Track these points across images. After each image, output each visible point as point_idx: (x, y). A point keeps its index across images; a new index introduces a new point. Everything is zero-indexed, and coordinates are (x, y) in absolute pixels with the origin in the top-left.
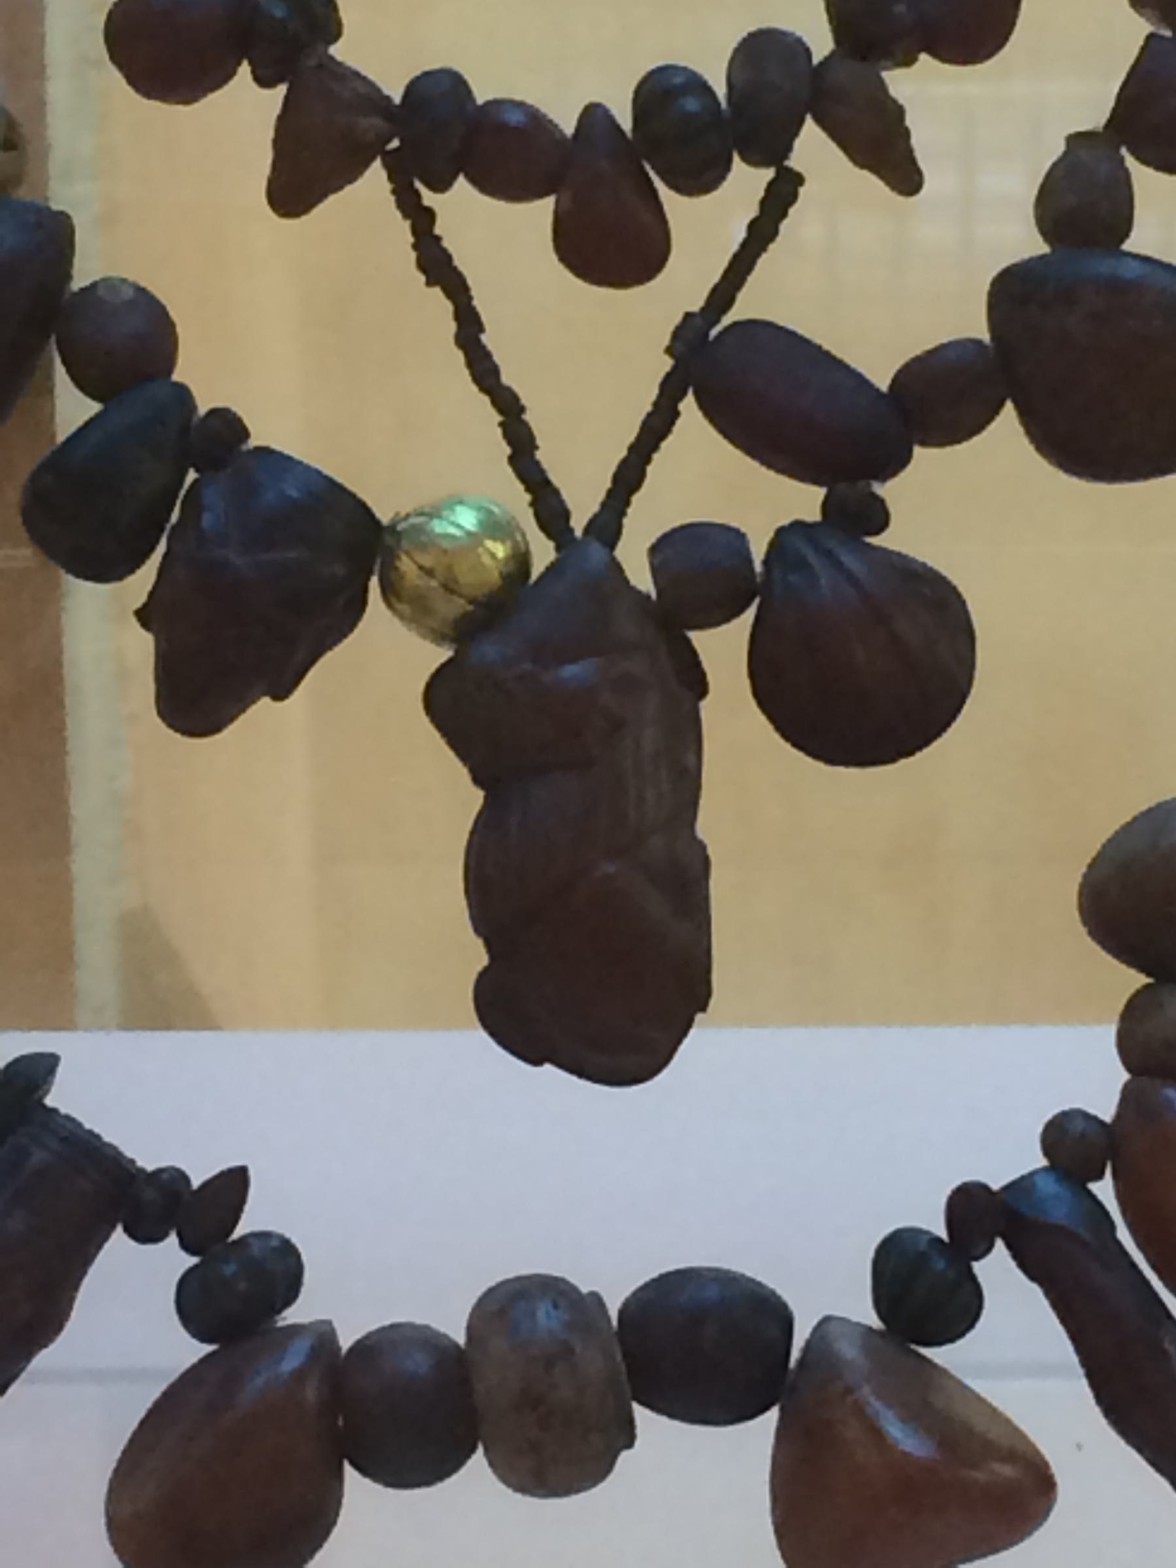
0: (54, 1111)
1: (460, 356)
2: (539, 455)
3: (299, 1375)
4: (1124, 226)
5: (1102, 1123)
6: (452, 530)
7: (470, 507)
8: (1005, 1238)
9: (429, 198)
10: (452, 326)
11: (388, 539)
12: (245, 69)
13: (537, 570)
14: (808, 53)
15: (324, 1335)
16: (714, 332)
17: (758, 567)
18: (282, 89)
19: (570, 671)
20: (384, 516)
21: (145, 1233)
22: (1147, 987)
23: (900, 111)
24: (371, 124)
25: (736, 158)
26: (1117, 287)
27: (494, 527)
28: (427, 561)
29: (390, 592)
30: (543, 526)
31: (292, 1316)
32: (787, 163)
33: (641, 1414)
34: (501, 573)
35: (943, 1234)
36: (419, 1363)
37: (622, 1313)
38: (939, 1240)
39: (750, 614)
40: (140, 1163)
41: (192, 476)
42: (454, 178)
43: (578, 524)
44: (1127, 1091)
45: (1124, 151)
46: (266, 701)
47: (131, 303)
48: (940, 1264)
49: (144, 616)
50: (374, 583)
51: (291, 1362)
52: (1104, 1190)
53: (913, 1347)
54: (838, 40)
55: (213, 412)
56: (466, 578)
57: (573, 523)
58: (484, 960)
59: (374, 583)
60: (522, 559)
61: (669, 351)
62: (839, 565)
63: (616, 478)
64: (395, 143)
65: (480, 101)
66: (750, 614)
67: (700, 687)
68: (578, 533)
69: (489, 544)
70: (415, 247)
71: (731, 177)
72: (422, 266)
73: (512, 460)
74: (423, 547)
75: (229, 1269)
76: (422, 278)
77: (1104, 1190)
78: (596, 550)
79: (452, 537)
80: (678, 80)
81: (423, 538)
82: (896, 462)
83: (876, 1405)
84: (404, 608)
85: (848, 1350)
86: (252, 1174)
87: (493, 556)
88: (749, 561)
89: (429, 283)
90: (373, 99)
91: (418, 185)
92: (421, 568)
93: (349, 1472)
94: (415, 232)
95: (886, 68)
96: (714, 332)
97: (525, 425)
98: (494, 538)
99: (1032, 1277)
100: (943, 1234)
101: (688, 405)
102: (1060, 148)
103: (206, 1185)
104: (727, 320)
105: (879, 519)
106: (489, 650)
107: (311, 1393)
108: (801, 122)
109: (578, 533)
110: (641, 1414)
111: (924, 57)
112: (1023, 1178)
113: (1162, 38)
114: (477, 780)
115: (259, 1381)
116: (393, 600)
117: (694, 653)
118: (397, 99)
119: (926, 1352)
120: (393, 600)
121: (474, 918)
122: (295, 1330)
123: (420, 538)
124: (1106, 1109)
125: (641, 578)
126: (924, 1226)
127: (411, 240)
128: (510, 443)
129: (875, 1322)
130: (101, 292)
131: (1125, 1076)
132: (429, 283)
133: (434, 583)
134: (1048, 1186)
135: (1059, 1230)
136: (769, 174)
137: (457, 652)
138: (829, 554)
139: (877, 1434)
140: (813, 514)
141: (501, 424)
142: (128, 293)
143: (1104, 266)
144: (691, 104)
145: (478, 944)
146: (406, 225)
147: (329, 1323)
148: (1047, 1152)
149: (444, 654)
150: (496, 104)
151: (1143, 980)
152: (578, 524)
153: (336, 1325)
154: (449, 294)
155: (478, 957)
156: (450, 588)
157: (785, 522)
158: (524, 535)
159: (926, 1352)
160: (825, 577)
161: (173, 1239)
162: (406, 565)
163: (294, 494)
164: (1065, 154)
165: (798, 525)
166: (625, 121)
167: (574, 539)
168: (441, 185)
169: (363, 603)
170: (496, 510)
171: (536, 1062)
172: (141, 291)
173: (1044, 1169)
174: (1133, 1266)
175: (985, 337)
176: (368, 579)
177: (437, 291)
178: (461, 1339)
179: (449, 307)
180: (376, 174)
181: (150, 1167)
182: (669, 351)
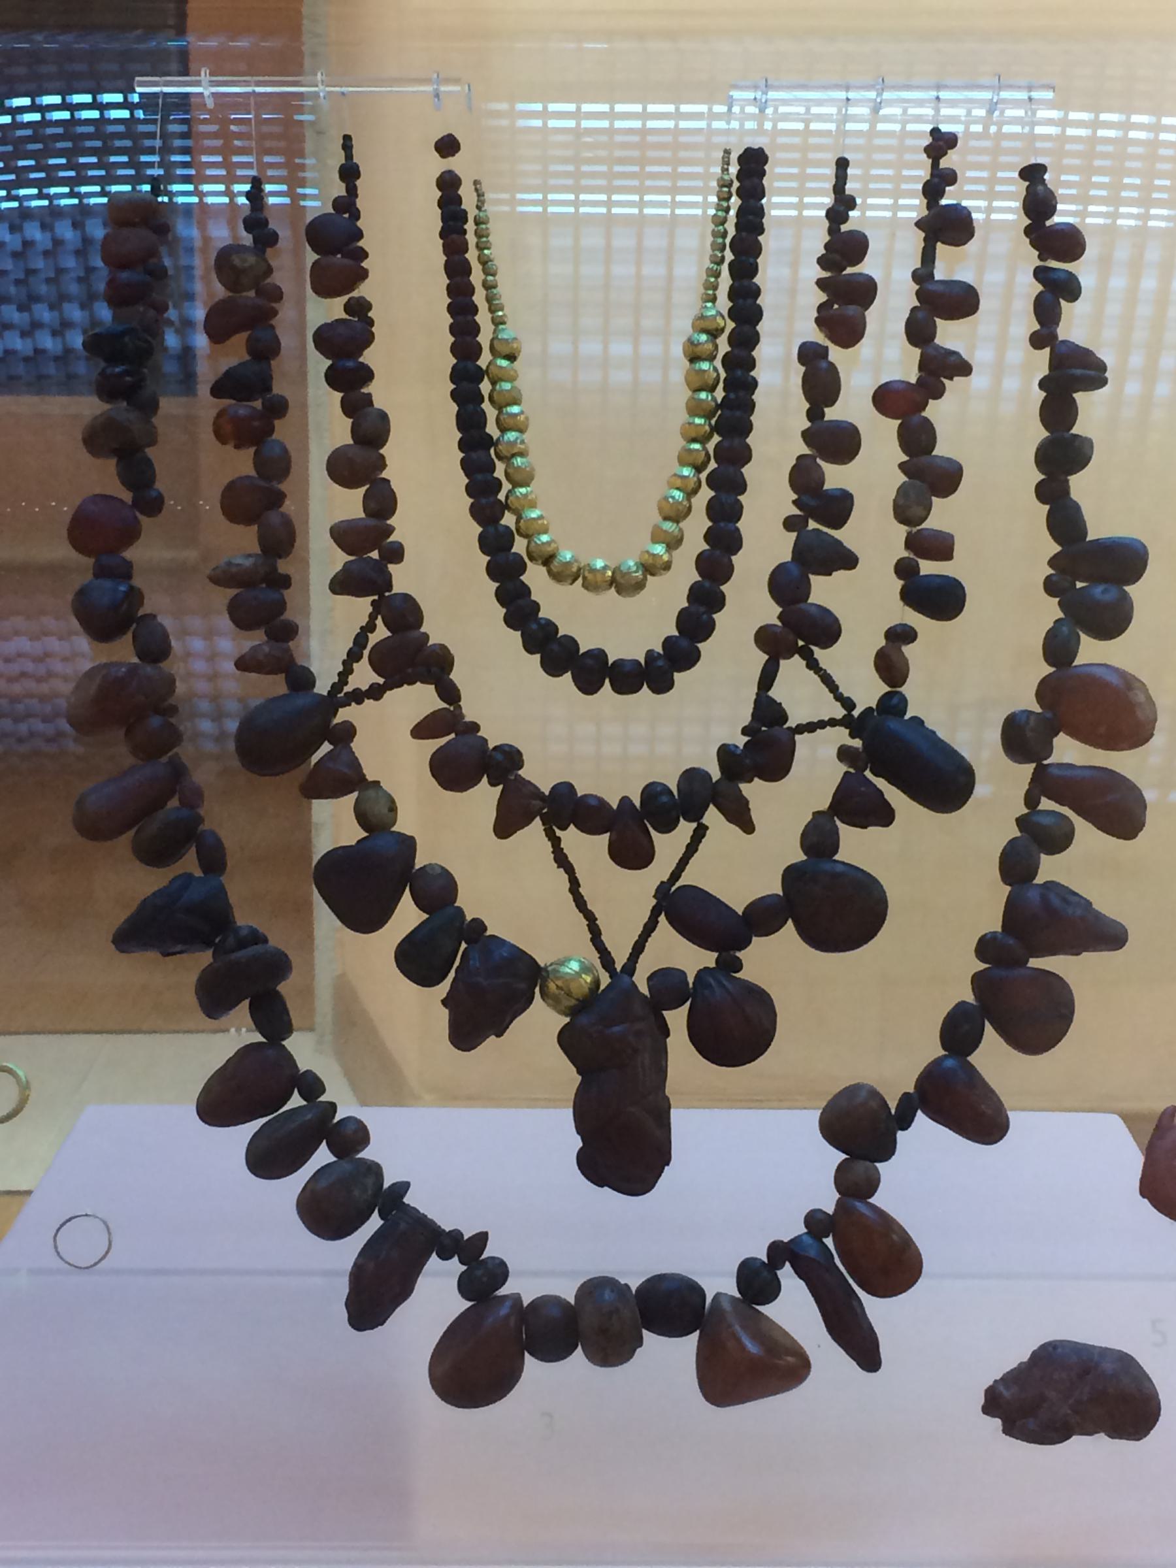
0: (408, 1205)
1: (571, 897)
2: (603, 938)
3: (507, 1317)
4: (835, 850)
5: (829, 1214)
6: (569, 971)
7: (575, 961)
8: (790, 1262)
9: (558, 833)
10: (568, 885)
11: (544, 974)
12: (485, 779)
13: (602, 987)
14: (711, 778)
15: (517, 1298)
16: (673, 889)
17: (691, 985)
18: (501, 787)
19: (616, 1029)
20: (542, 965)
21: (445, 1256)
22: (846, 1159)
23: (747, 802)
24: (537, 803)
25: (681, 819)
26: (835, 876)
27: (586, 969)
28: (560, 983)
29: (544, 995)
30: (604, 967)
31: (503, 1291)
32: (701, 821)
33: (645, 1332)
34: (589, 988)
35: (766, 1260)
36: (555, 1312)
37: (636, 1291)
38: (764, 1262)
39: (688, 1004)
40: (443, 1227)
41: (464, 946)
42: (569, 825)
43: (619, 967)
44: (839, 1202)
45: (836, 818)
46: (493, 1037)
47: (440, 875)
48: (765, 1274)
49: (445, 1002)
50: (537, 990)
51: (504, 1311)
52: (829, 1242)
53: (754, 1306)
54: (722, 773)
55: (474, 920)
56: (574, 988)
57: (616, 966)
58: (581, 1144)
59: (537, 990)
60: (597, 982)
61: (654, 896)
62: (724, 986)
63: (633, 948)
64: (545, 810)
65: (579, 795)
66: (688, 1004)
67: (667, 1033)
68: (619, 970)
69: (583, 976)
70: (553, 852)
71: (680, 825)
72: (556, 860)
73: (592, 940)
74: (558, 978)
75: (479, 1273)
76: (556, 865)
77: (829, 1242)
78: (626, 978)
79: (568, 973)
80: (659, 789)
81: (558, 975)
82: (744, 943)
83: (737, 1328)
84: (550, 1001)
85: (726, 1305)
86: (411, 1183)
87: (586, 982)
88: (687, 984)
89: (558, 867)
90: (536, 792)
91: (554, 828)
92: (557, 986)
93: (526, 1354)
94: (553, 846)
95: (741, 783)
96: (673, 889)
97: (597, 926)
98: (586, 974)
99: (801, 1277)
100: (766, 1260)
101: (662, 918)
102: (809, 817)
103: (470, 1239)
104: (678, 884)
105: (738, 966)
106: (584, 1020)
107: (512, 1321)
108: (708, 806)
109: (619, 970)
110: (645, 1332)
111: (756, 780)
112: (796, 1238)
113: (850, 773)
114: (579, 1072)
115: (490, 1320)
116: (545, 998)
117: (664, 1018)
118: (547, 793)
119: (758, 1307)
120: (545, 998)
121: (577, 1128)
122: (505, 1298)
123: (557, 974)
124: (830, 1209)
125: (644, 989)
126: (759, 1257)
127: (552, 850)
128: (591, 933)
129: (738, 1295)
130: (427, 869)
131: (837, 1196)
132: (558, 867)
133: (563, 992)
134: (808, 1240)
135: (814, 1260)
136: (695, 825)
137: (571, 1020)
138: (720, 983)
139: (743, 1348)
140: (712, 965)
141: (588, 925)
142: (439, 871)
143: (827, 866)
144: (665, 799)
145: (579, 1138)
146: (549, 844)
147: (519, 1294)
148: (806, 1227)
149: (567, 1020)
150: (585, 796)
151: (844, 1156)
152: (619, 967)
153: (522, 1295)
154: (566, 872)
155: (579, 1143)
156: (569, 994)
157: (702, 967)
158: (597, 971)
159: (759, 1308)
160: (718, 991)
161: (456, 1258)
162: (552, 986)
163: (505, 954)
164: (812, 820)
165: (706, 969)
166: (637, 802)
167: (617, 973)
168: (564, 828)
169: (533, 998)
170: (586, 962)
171: (602, 1186)
172: (443, 868)
173: (806, 1233)
174: (842, 1274)
175: (781, 893)
176: (534, 989)
177: (562, 870)
178: (572, 1302)
179: (566, 876)
180: (538, 821)
181: (447, 1230)
182: (654, 896)
